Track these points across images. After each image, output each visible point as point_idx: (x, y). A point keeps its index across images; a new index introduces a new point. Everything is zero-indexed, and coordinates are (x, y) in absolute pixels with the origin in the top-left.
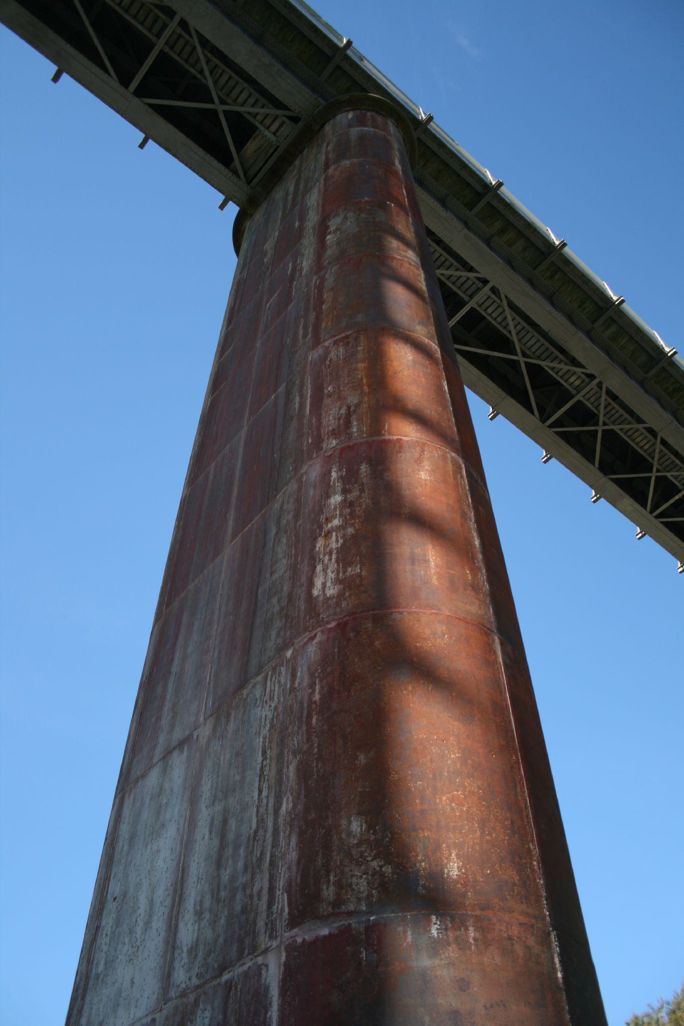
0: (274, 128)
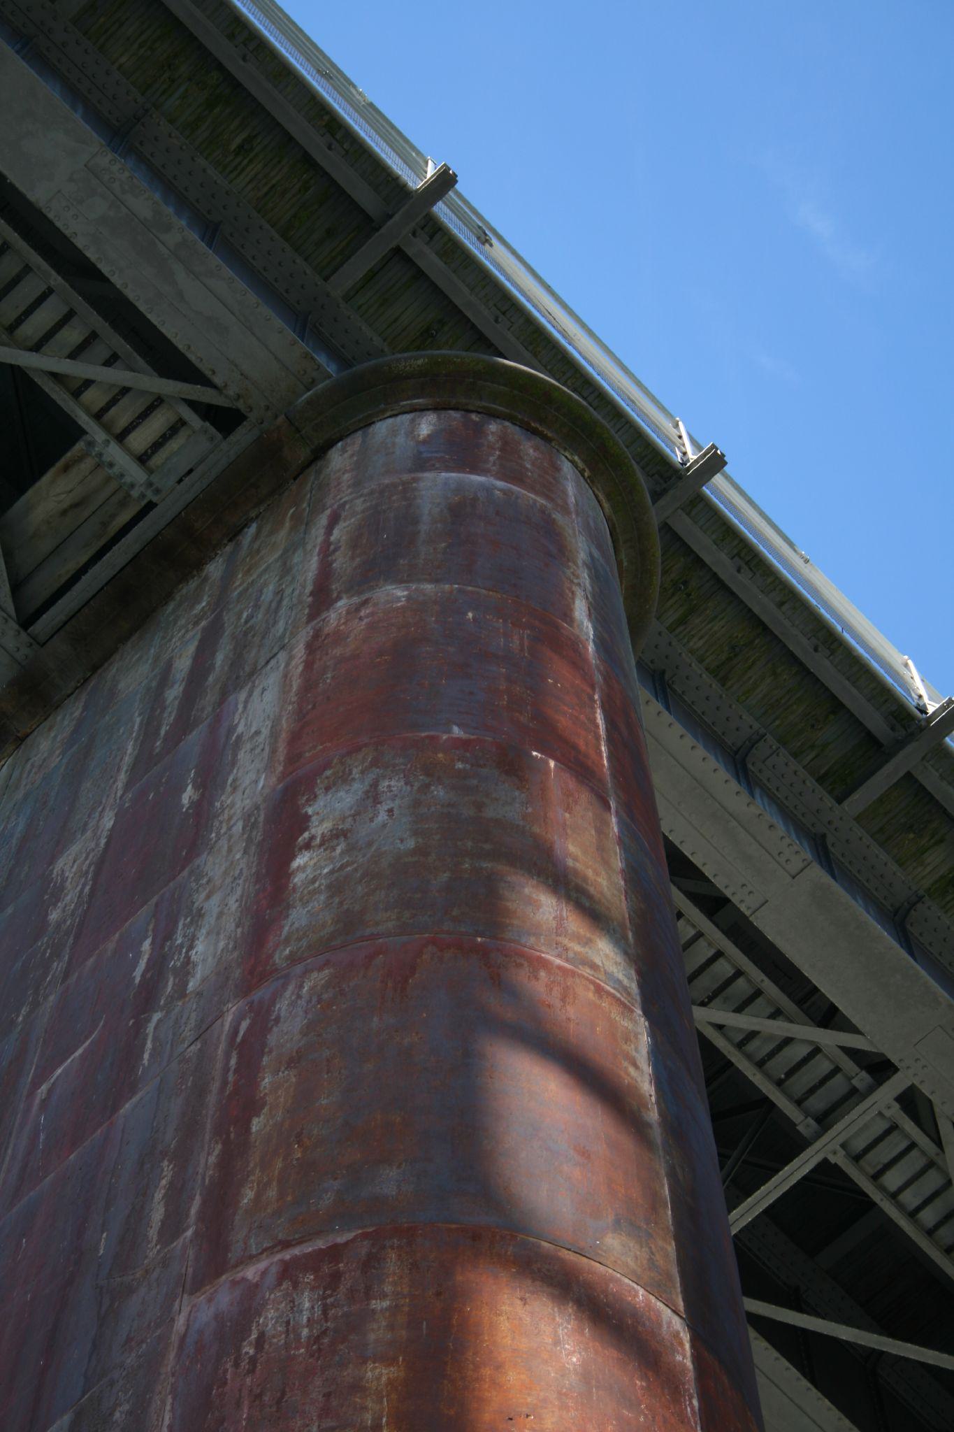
0: (141, 439)
